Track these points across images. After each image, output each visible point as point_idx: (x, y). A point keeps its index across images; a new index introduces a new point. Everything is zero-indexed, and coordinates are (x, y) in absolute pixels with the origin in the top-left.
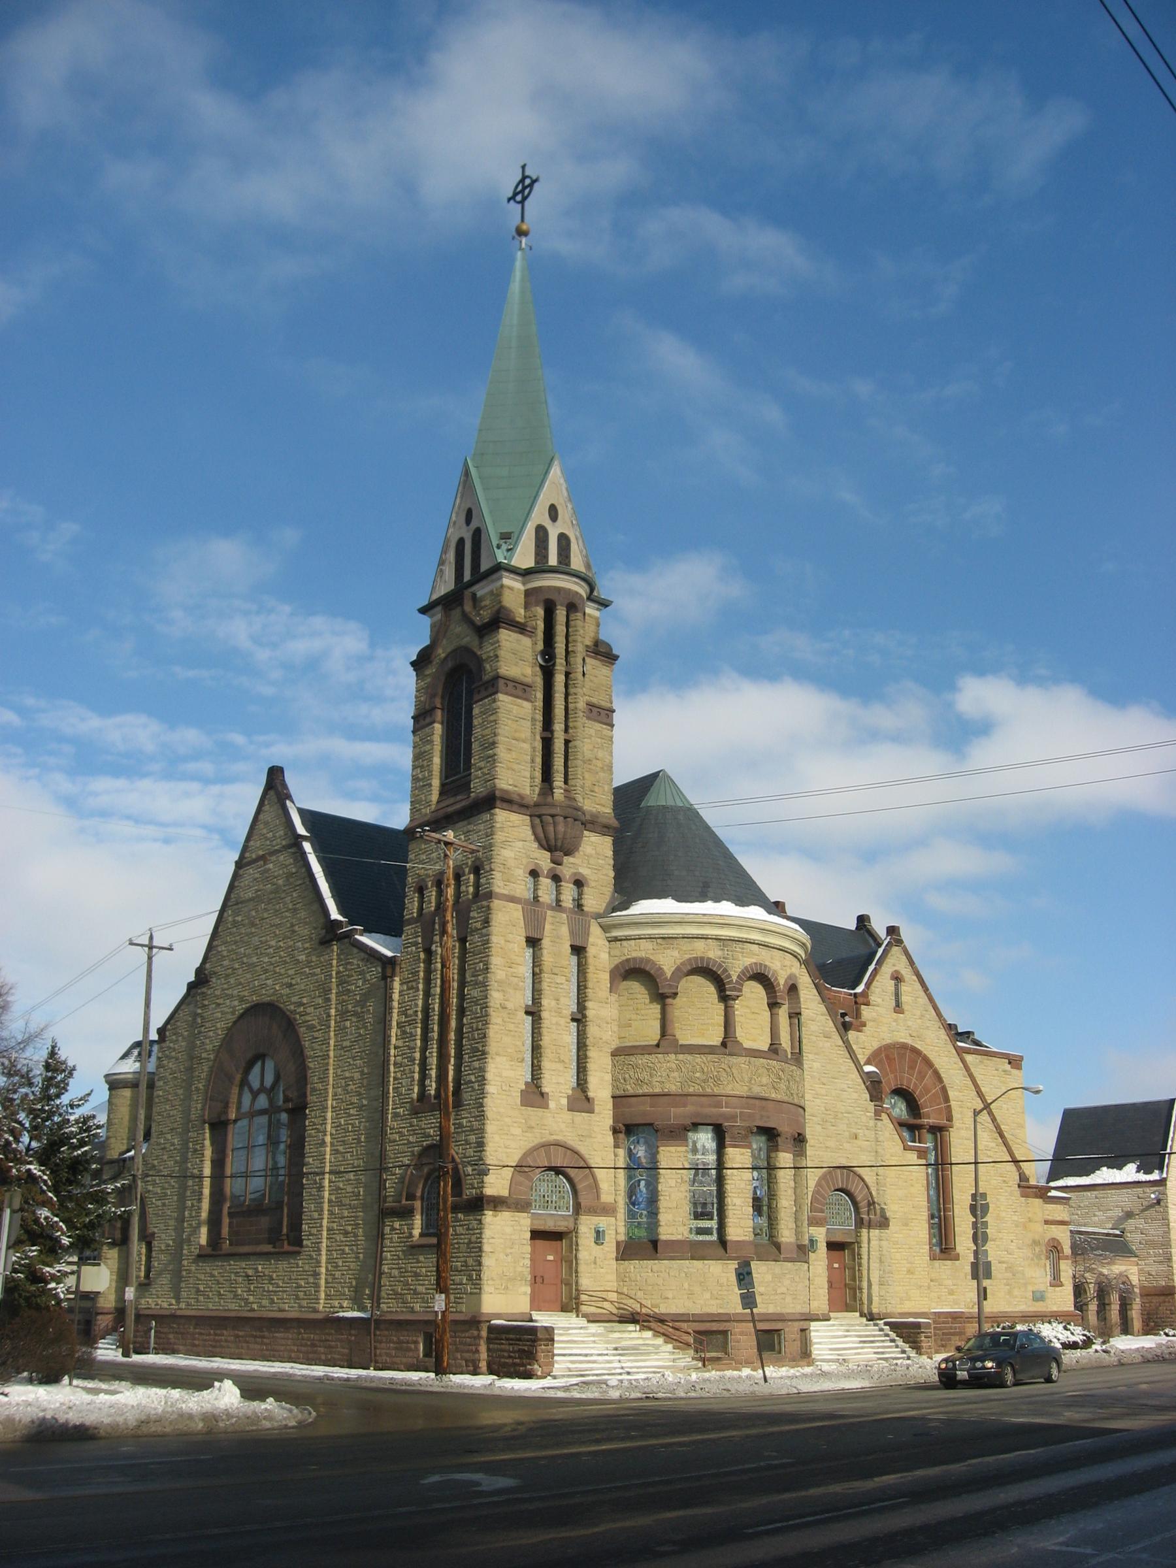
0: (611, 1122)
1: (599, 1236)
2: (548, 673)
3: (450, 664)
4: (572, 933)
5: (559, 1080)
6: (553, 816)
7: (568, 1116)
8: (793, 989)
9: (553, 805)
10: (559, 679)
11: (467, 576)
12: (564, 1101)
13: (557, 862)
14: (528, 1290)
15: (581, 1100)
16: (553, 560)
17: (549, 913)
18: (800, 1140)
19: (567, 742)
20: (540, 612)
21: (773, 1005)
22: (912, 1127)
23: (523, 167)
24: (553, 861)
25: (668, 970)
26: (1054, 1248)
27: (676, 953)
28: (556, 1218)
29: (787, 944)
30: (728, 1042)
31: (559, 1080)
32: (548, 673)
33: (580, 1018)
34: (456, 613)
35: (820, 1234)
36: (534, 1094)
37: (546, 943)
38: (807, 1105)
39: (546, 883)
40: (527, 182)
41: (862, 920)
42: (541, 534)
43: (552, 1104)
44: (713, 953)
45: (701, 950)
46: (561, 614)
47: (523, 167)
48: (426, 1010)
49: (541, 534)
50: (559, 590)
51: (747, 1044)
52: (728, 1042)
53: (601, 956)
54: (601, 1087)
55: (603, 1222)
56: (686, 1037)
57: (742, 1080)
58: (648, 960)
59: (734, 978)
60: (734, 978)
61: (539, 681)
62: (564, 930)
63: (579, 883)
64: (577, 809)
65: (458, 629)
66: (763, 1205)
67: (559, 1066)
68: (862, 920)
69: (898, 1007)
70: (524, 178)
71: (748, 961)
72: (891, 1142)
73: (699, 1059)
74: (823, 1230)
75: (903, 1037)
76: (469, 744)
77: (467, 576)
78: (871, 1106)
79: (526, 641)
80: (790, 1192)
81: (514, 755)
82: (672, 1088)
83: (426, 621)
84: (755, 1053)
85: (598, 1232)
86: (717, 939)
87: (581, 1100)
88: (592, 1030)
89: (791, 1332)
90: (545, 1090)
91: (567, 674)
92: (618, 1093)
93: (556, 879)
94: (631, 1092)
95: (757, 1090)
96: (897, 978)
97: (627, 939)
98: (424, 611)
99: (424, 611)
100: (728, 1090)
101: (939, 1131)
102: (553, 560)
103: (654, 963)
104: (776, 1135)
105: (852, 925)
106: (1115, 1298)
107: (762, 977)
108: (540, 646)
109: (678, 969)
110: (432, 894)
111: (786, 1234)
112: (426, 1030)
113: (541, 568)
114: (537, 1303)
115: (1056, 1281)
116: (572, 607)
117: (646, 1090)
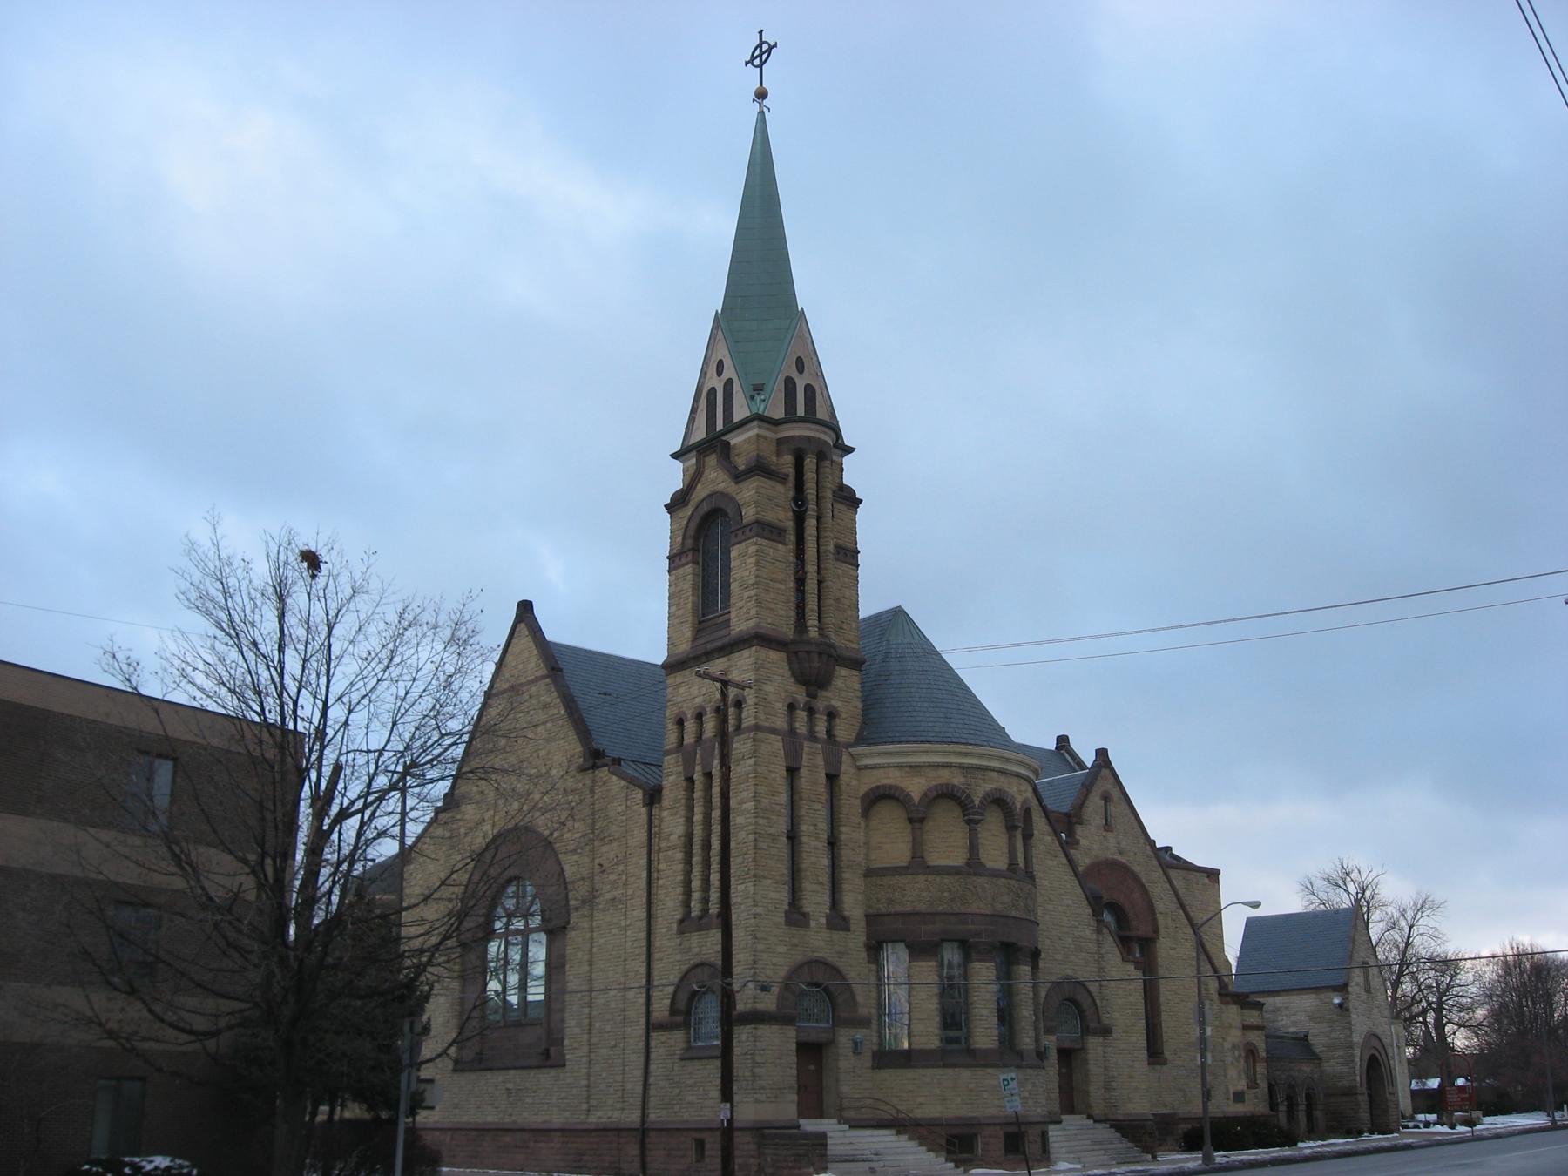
0: (863, 939)
1: (856, 1047)
2: (800, 519)
3: (705, 508)
4: (827, 763)
5: (816, 901)
6: (808, 652)
7: (826, 934)
8: (1027, 812)
9: (809, 643)
10: (811, 523)
11: (720, 426)
12: (823, 920)
13: (814, 696)
14: (795, 1097)
15: (838, 921)
16: (801, 411)
17: (806, 744)
18: (1035, 955)
19: (820, 582)
20: (789, 459)
21: (1011, 828)
22: (1124, 942)
23: (761, 33)
24: (808, 695)
25: (916, 796)
26: (1251, 1052)
27: (923, 781)
28: (815, 1029)
29: (1022, 771)
30: (974, 865)
31: (816, 901)
32: (800, 519)
33: (833, 843)
34: (712, 460)
35: (1050, 1042)
36: (796, 916)
37: (804, 771)
38: (1039, 920)
39: (802, 715)
40: (765, 47)
41: (1063, 741)
42: (790, 384)
43: (813, 924)
44: (958, 780)
45: (945, 776)
46: (810, 462)
47: (761, 33)
48: (689, 836)
49: (790, 384)
50: (809, 439)
51: (989, 865)
52: (974, 865)
53: (854, 785)
54: (853, 906)
55: (859, 1034)
56: (935, 859)
57: (987, 898)
58: (897, 788)
59: (977, 803)
60: (977, 803)
61: (790, 524)
62: (820, 760)
63: (831, 715)
64: (831, 646)
65: (713, 475)
66: (1006, 1015)
67: (818, 888)
68: (1063, 741)
69: (1107, 826)
70: (762, 43)
71: (989, 787)
72: (1112, 954)
73: (947, 880)
74: (1053, 1038)
75: (1112, 854)
76: (726, 586)
77: (720, 426)
78: (1093, 922)
79: (780, 488)
80: (1030, 1002)
81: (772, 595)
82: (922, 907)
83: (678, 466)
84: (995, 874)
85: (855, 1043)
86: (961, 766)
87: (838, 921)
88: (846, 854)
89: (1033, 1134)
90: (846, 913)
91: (819, 519)
92: (871, 911)
93: (811, 711)
94: (884, 910)
95: (999, 908)
96: (1106, 798)
97: (875, 767)
98: (675, 456)
99: (675, 456)
100: (973, 908)
101: (1148, 943)
102: (801, 411)
103: (902, 790)
104: (1013, 950)
105: (1052, 746)
106: (1301, 1099)
107: (999, 801)
108: (791, 494)
109: (925, 795)
110: (690, 726)
111: (1026, 1041)
112: (689, 854)
113: (791, 418)
114: (802, 1114)
115: (1252, 1084)
116: (821, 456)
117: (899, 909)
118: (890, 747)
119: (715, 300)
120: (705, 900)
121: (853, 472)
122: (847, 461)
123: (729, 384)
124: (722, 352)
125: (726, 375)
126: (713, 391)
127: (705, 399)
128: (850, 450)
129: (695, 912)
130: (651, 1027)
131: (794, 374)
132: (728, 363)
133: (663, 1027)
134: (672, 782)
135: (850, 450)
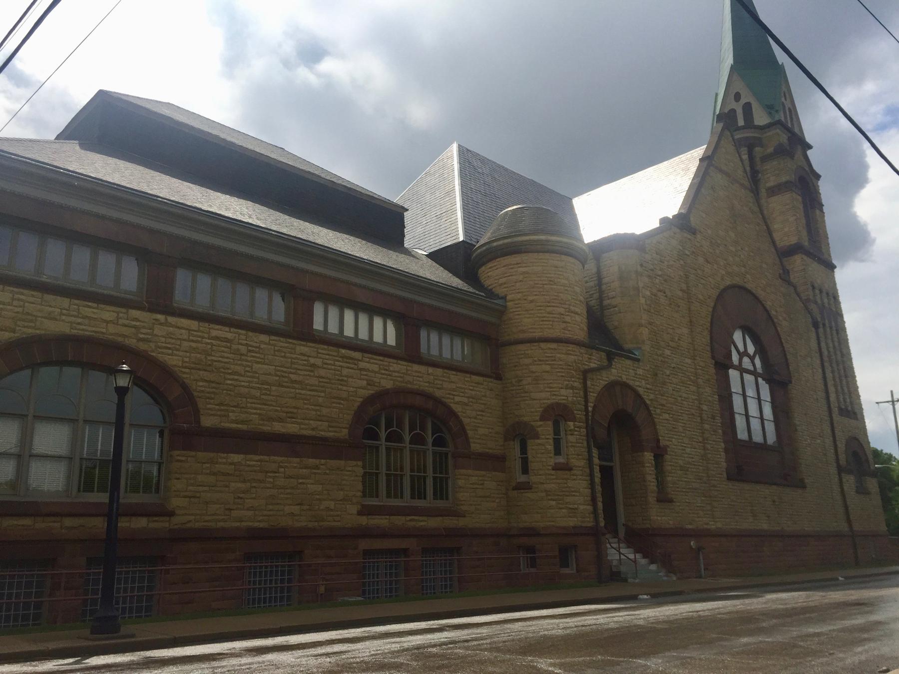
122: (809, 152)
123: (747, 108)
125: (743, 100)
130: (840, 470)
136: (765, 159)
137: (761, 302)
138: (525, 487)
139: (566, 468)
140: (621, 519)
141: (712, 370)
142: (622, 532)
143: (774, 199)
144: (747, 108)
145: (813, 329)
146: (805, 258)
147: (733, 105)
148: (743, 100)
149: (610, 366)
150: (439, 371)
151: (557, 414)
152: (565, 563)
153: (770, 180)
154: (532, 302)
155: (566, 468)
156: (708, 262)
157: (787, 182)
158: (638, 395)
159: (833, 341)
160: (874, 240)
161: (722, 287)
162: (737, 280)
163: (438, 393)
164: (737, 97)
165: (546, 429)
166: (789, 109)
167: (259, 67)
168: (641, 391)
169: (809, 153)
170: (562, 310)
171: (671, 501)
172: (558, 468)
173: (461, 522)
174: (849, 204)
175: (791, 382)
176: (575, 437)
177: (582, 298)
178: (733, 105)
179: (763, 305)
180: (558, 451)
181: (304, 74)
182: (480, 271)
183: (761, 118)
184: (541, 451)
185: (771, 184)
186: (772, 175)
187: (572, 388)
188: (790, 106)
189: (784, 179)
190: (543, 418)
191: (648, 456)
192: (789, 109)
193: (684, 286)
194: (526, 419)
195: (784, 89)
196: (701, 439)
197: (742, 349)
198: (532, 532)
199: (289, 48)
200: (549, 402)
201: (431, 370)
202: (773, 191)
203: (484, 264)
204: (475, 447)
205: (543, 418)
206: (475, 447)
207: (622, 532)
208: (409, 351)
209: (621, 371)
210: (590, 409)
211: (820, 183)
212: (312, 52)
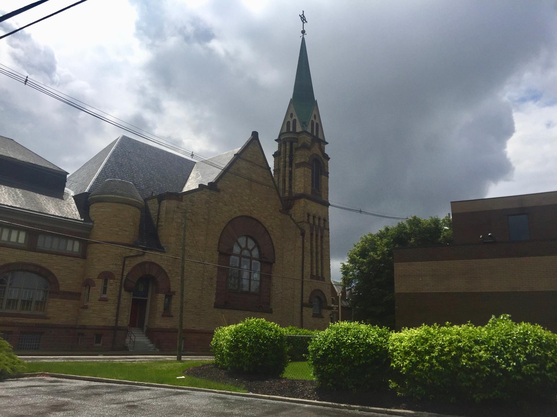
16: (291, 130)
102: (291, 130)
118: (29, 321)
119: (291, 96)
120: (317, 271)
121: (328, 150)
122: (326, 146)
123: (295, 121)
124: (293, 111)
125: (294, 118)
126: (289, 122)
127: (287, 123)
128: (327, 143)
129: (315, 274)
130: (303, 305)
131: (314, 119)
132: (294, 114)
133: (307, 306)
134: (308, 232)
135: (327, 143)
136: (297, 149)
137: (261, 223)
138: (86, 307)
139: (106, 300)
140: (146, 323)
141: (216, 256)
142: (145, 329)
143: (298, 169)
144: (295, 121)
145: (301, 236)
146: (307, 201)
147: (289, 119)
148: (294, 118)
149: (144, 254)
150: (46, 255)
151: (106, 276)
152: (98, 341)
153: (298, 160)
154: (104, 225)
155: (106, 300)
156: (225, 205)
157: (305, 162)
158: (160, 267)
159: (317, 242)
160: (514, 169)
161: (233, 217)
162: (247, 213)
163: (44, 265)
164: (292, 115)
165: (99, 283)
166: (317, 124)
167: (172, 42)
168: (163, 266)
169: (326, 147)
170: (117, 229)
171: (172, 316)
172: (102, 300)
173: (47, 321)
174: (504, 146)
175: (274, 262)
176: (113, 286)
177: (132, 224)
178: (289, 119)
179: (263, 226)
180: (105, 292)
181: (197, 46)
182: (92, 206)
183: (299, 129)
184: (96, 292)
185: (297, 162)
186: (301, 157)
187: (116, 265)
188: (318, 122)
189: (303, 160)
190: (98, 278)
191: (161, 297)
192: (317, 124)
193: (206, 217)
194: (91, 277)
195: (315, 112)
196: (200, 288)
197: (243, 246)
198: (84, 327)
199: (190, 29)
200: (103, 271)
201: (40, 254)
202: (298, 165)
203: (93, 203)
204: (62, 288)
205: (98, 278)
206: (62, 288)
207: (145, 329)
208: (31, 246)
209: (152, 256)
210: (125, 274)
211: (329, 162)
212: (205, 35)
